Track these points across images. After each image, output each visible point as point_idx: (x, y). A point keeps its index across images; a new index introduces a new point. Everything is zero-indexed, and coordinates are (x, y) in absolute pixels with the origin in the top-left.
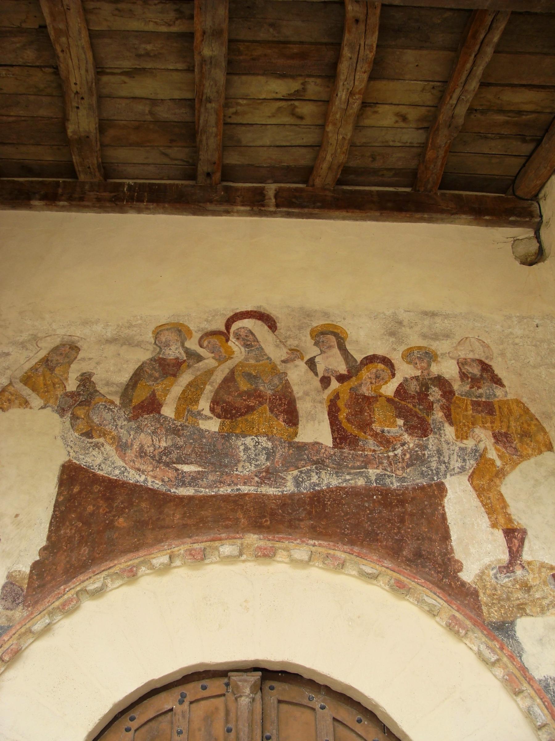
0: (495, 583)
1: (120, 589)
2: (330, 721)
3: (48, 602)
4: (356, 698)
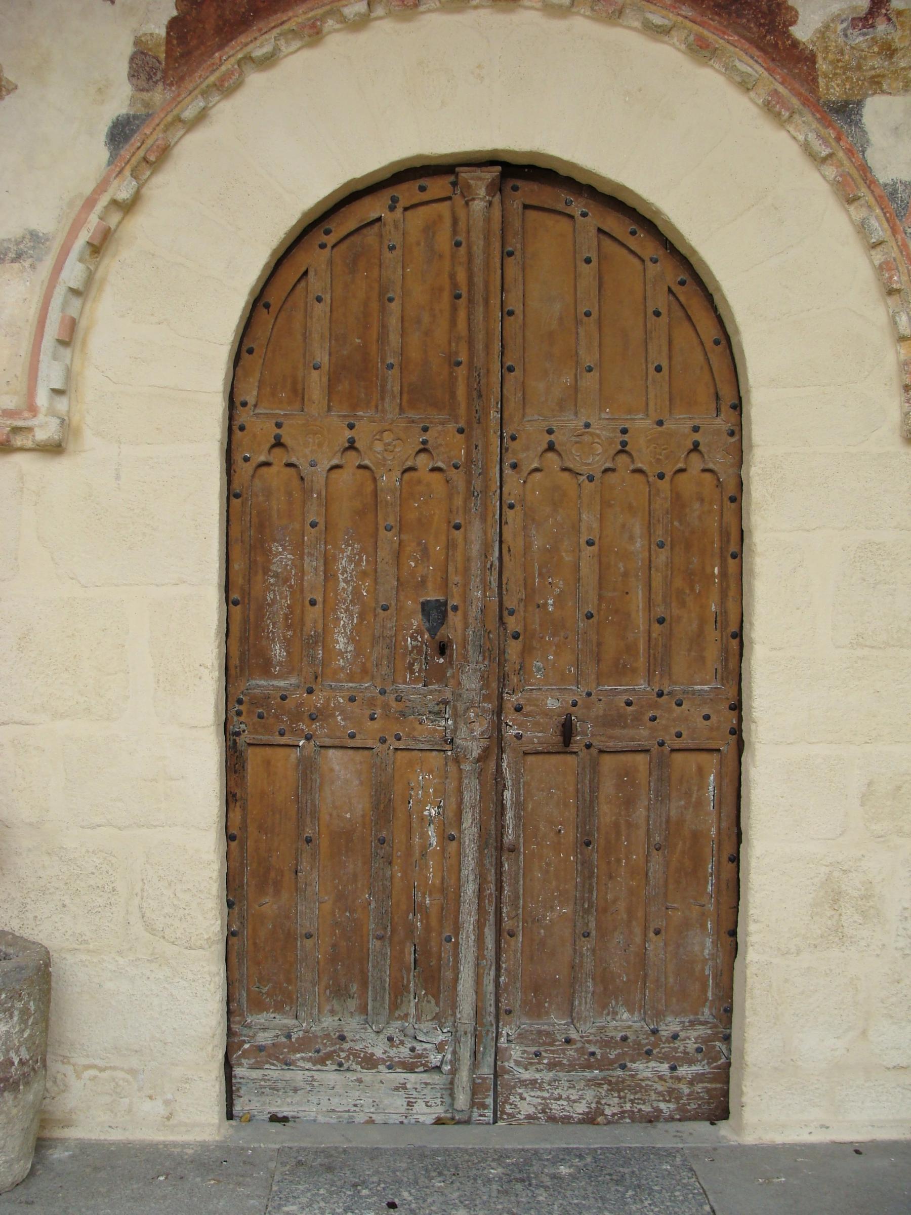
0: (843, 44)
1: (299, 53)
2: (593, 232)
3: (201, 76)
4: (630, 202)
